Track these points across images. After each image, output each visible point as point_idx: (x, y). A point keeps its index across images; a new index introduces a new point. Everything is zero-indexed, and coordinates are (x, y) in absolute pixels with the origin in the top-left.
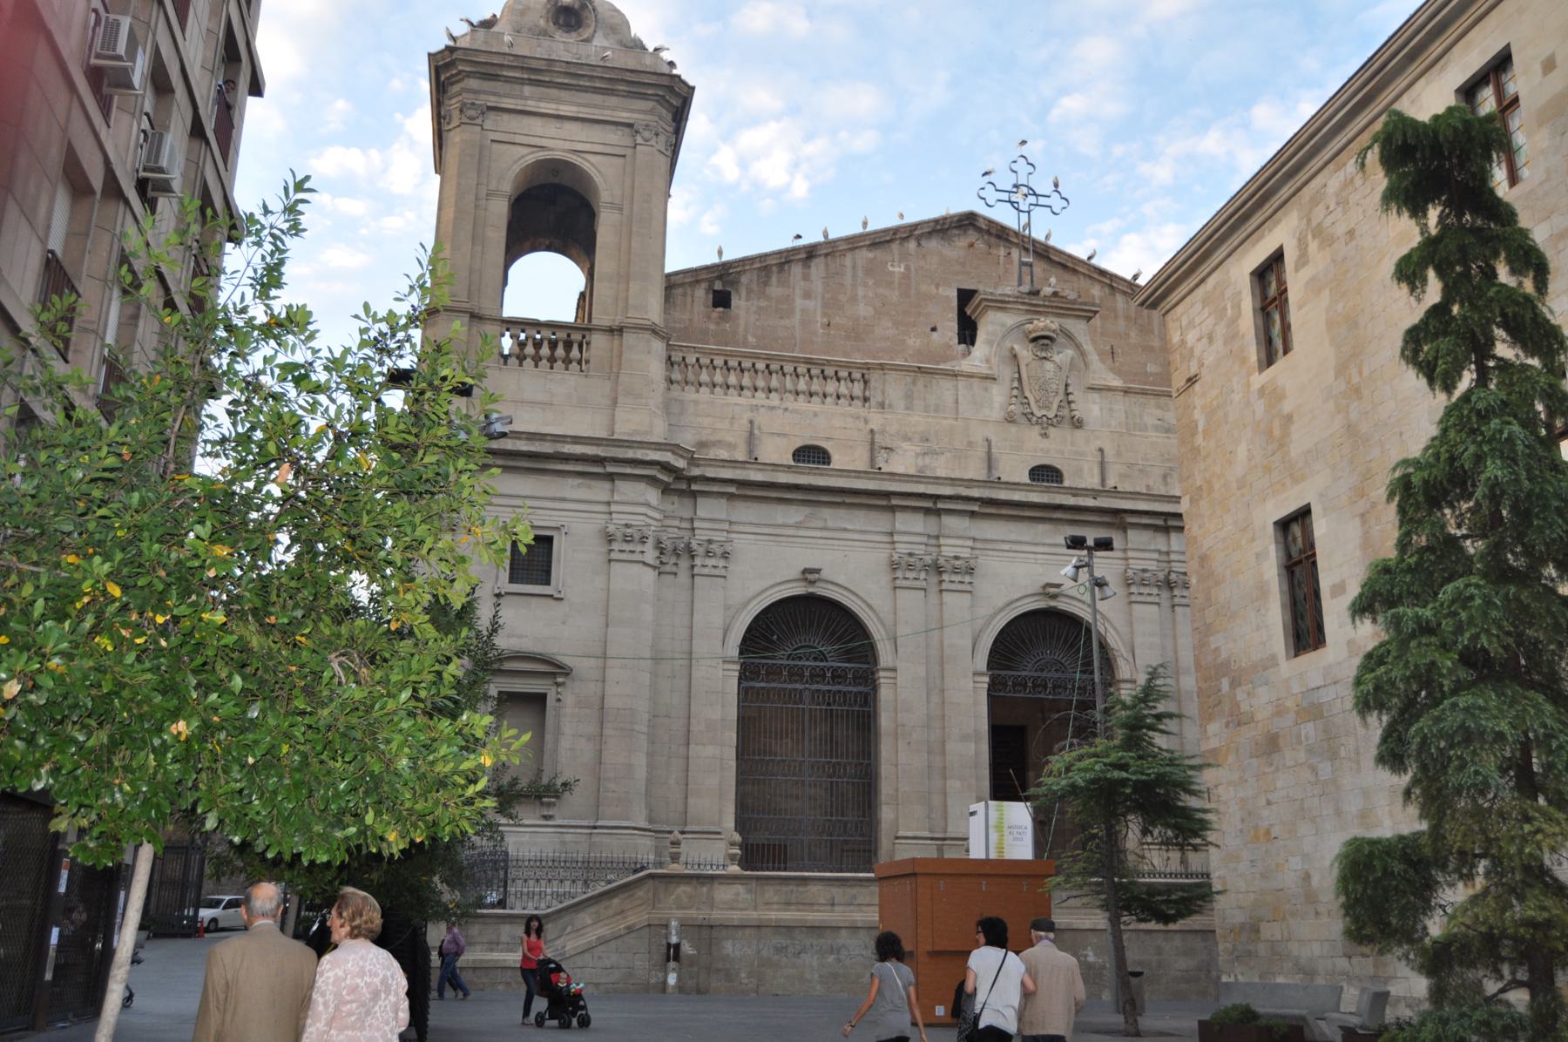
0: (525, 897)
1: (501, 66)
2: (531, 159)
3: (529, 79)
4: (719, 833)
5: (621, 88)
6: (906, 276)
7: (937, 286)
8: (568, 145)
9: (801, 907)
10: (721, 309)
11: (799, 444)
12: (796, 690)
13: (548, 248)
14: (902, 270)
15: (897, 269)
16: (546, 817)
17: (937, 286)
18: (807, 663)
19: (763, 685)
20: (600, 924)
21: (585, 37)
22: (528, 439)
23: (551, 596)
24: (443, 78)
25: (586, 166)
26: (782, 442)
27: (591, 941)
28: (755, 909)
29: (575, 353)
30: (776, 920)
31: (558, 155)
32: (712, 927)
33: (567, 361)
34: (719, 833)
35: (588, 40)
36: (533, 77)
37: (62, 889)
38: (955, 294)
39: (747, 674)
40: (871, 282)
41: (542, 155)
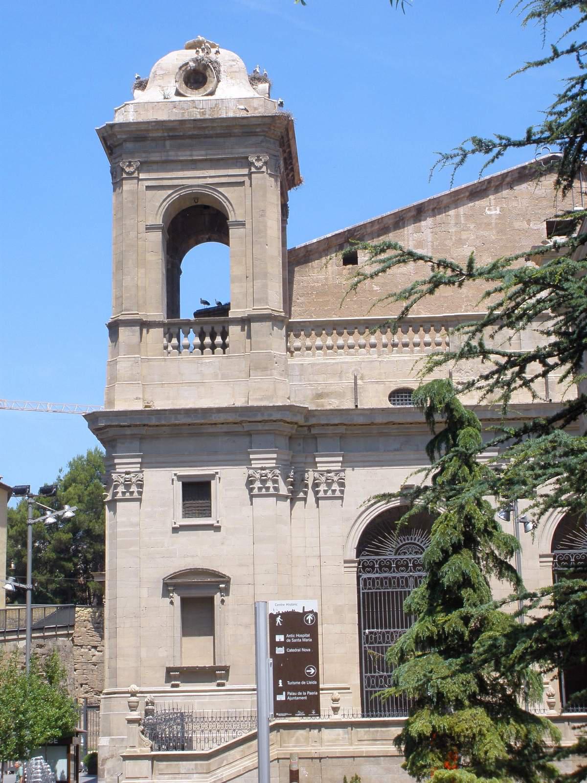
0: (211, 742)
2: (175, 196)
3: (169, 136)
4: (349, 689)
6: (500, 217)
7: (529, 221)
9: (384, 742)
10: (350, 266)
11: (394, 387)
12: (402, 577)
13: (209, 240)
14: (498, 212)
15: (493, 212)
16: (219, 685)
17: (529, 221)
18: (410, 557)
19: (377, 575)
20: (246, 759)
21: (209, 91)
23: (212, 525)
24: (108, 144)
26: (381, 387)
27: (240, 770)
28: (351, 744)
29: (219, 340)
30: (367, 752)
32: (320, 758)
33: (213, 347)
34: (349, 689)
35: (212, 93)
37: (309, 650)
38: (545, 225)
39: (363, 567)
40: (472, 226)
41: (183, 192)
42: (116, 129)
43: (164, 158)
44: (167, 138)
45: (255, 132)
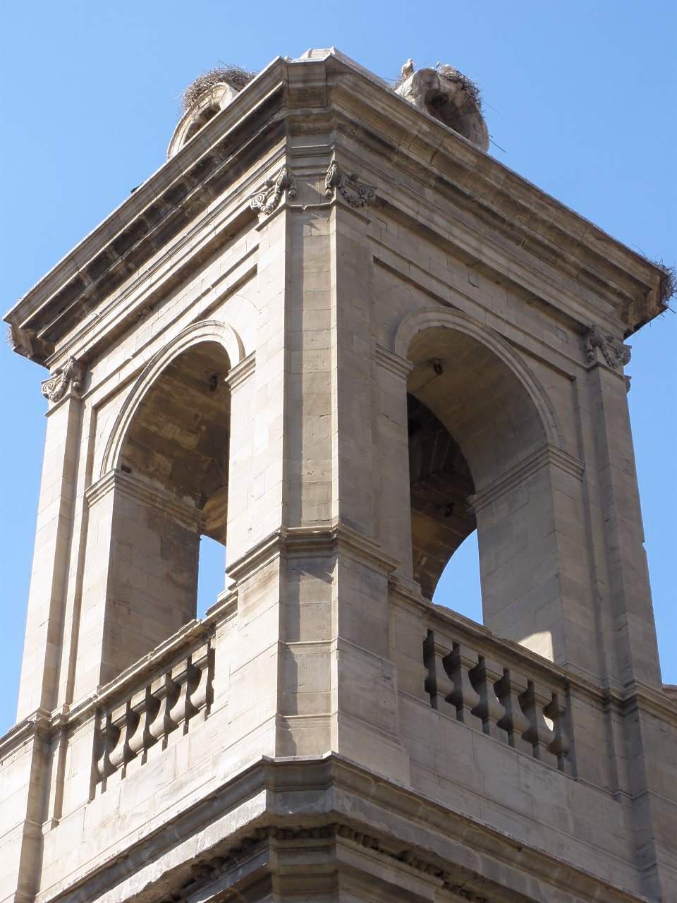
1: (403, 132)
3: (440, 180)
5: (572, 258)
8: (490, 321)
22: (561, 884)
25: (517, 368)
31: (474, 331)
36: (446, 178)
41: (449, 319)
42: (345, 82)
43: (421, 220)
44: (433, 182)
45: (605, 285)
